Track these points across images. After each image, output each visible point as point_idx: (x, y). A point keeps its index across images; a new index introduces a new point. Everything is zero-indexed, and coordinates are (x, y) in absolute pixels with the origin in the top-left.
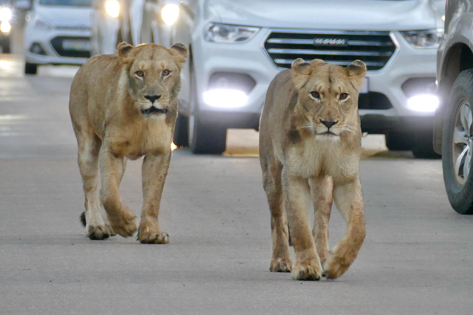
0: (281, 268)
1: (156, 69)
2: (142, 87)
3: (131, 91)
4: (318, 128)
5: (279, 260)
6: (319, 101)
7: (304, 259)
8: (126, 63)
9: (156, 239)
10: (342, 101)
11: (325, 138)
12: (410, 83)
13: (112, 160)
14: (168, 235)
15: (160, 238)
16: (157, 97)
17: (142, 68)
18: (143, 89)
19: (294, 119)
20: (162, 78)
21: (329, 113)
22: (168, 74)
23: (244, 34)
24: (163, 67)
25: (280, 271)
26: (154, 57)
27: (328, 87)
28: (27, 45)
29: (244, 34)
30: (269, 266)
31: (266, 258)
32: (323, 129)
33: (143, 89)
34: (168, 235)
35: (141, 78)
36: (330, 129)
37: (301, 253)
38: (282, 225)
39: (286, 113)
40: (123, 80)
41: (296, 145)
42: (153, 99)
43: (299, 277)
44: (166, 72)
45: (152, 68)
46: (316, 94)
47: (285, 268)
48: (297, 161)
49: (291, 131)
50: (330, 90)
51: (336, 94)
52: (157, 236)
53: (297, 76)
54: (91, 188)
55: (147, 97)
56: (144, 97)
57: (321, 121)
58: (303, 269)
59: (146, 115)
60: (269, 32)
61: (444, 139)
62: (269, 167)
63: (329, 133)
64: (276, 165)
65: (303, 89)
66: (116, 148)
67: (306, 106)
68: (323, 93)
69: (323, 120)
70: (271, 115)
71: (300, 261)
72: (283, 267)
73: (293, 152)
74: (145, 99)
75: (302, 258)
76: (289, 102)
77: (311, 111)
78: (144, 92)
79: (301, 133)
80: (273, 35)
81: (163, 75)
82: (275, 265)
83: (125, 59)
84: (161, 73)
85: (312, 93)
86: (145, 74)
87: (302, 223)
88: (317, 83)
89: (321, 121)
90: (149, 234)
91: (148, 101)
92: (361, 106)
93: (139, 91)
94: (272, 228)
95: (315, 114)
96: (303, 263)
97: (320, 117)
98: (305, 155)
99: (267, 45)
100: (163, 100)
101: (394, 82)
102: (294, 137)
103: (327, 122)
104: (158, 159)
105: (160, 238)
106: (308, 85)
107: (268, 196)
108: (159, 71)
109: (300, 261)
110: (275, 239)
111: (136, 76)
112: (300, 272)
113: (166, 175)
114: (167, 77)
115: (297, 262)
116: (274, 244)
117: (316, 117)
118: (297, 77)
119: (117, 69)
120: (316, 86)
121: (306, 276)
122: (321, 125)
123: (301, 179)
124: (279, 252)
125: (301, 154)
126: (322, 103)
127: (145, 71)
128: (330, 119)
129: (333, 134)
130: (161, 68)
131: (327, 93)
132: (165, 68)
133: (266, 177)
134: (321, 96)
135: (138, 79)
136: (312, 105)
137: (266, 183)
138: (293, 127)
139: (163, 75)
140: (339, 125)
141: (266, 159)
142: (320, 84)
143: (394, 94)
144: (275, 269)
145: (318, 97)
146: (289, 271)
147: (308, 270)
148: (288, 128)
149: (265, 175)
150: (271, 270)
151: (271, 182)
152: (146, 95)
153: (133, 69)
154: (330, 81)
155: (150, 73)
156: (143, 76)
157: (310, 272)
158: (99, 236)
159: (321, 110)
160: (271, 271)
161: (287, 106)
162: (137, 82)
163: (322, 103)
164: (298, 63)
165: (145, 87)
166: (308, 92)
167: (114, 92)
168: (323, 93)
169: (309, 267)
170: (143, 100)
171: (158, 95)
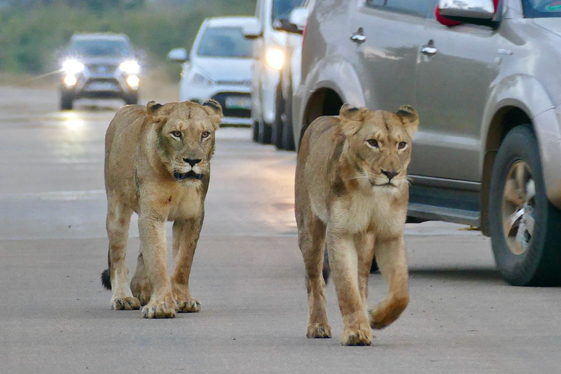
0: (319, 334)
1: (196, 130)
2: (181, 148)
3: (161, 152)
4: (378, 178)
5: (317, 325)
6: (378, 149)
7: (353, 323)
8: (158, 122)
9: (185, 307)
11: (385, 189)
14: (198, 304)
15: (189, 306)
16: (198, 161)
18: (182, 152)
19: (339, 169)
20: (202, 140)
21: (392, 163)
22: (208, 135)
25: (318, 337)
26: (191, 116)
27: (387, 135)
30: (306, 333)
31: (303, 324)
32: (384, 179)
33: (182, 152)
34: (198, 304)
35: (178, 139)
36: (391, 180)
37: (349, 317)
38: (320, 287)
39: (330, 164)
41: (342, 198)
42: (193, 163)
43: (349, 343)
44: (206, 133)
45: (192, 129)
46: (374, 142)
47: (323, 333)
48: (343, 215)
49: (335, 183)
50: (389, 139)
53: (346, 122)
54: (119, 259)
55: (187, 161)
57: (382, 172)
58: (353, 333)
62: (306, 222)
63: (389, 184)
64: (313, 220)
65: (355, 136)
67: (362, 155)
68: (382, 142)
69: (385, 170)
70: (307, 165)
71: (349, 325)
72: (321, 332)
73: (338, 206)
74: (184, 162)
75: (350, 322)
76: (332, 152)
77: (367, 160)
78: (184, 154)
79: (347, 184)
81: (202, 137)
82: (312, 331)
84: (201, 134)
85: (369, 141)
86: (183, 134)
87: (350, 284)
89: (382, 172)
91: (187, 164)
93: (175, 153)
94: (309, 291)
95: (373, 164)
96: (352, 327)
97: (381, 168)
98: (351, 209)
100: (203, 165)
102: (339, 189)
103: (389, 172)
105: (189, 306)
106: (363, 132)
107: (304, 255)
108: (199, 132)
109: (349, 325)
110: (312, 303)
111: (172, 135)
112: (350, 337)
113: (196, 241)
114: (206, 139)
115: (346, 327)
116: (311, 308)
117: (375, 166)
118: (347, 124)
120: (374, 134)
121: (357, 341)
122: (383, 175)
123: (345, 234)
124: (318, 316)
125: (348, 208)
126: (381, 152)
128: (394, 170)
129: (393, 185)
130: (201, 129)
131: (386, 141)
132: (206, 129)
133: (302, 234)
134: (380, 144)
136: (369, 154)
137: (302, 241)
138: (339, 178)
139: (202, 137)
140: (401, 176)
141: (302, 215)
142: (379, 132)
144: (313, 335)
146: (326, 337)
147: (358, 335)
148: (333, 179)
149: (301, 232)
150: (308, 336)
151: (308, 239)
152: (186, 158)
153: (167, 129)
155: (190, 134)
156: (180, 136)
157: (361, 337)
159: (381, 159)
160: (308, 337)
161: (330, 157)
162: (173, 143)
163: (381, 152)
164: (347, 109)
165: (185, 149)
166: (365, 140)
168: (382, 142)
169: (359, 331)
171: (200, 158)
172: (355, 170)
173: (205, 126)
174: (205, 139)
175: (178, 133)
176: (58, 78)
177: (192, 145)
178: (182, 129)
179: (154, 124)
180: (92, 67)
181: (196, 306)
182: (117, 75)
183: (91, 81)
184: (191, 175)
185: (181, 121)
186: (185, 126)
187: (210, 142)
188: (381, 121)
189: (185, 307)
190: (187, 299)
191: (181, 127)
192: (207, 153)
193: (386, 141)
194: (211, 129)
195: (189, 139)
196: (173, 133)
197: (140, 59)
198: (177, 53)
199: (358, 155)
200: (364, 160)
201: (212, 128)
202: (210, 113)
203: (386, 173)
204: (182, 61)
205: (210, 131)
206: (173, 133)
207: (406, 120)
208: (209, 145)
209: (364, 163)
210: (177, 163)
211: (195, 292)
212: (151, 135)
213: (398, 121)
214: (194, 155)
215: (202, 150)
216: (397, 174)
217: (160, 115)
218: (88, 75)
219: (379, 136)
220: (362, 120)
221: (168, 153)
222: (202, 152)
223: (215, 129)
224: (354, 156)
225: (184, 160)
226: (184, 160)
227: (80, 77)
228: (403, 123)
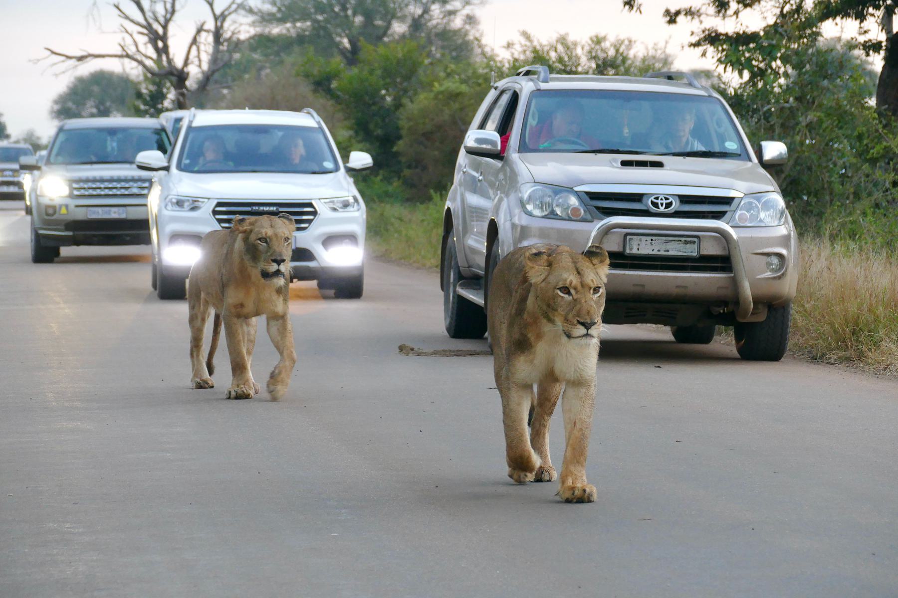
8: (244, 232)
12: (329, 240)
23: (197, 204)
28: (517, 87)
29: (197, 204)
32: (582, 330)
35: (265, 244)
50: (583, 285)
57: (579, 322)
60: (215, 202)
63: (587, 335)
69: (582, 321)
80: (219, 204)
88: (565, 275)
89: (579, 322)
92: (294, 259)
93: (263, 257)
98: (535, 362)
99: (215, 213)
101: (317, 239)
106: (552, 279)
120: (566, 280)
126: (575, 300)
131: (579, 287)
134: (573, 291)
143: (318, 250)
145: (569, 293)
148: (517, 336)
153: (253, 237)
154: (579, 273)
156: (266, 242)
162: (260, 248)
166: (555, 288)
168: (575, 289)
172: (544, 321)
179: (240, 235)
188: (571, 265)
193: (579, 287)
196: (260, 239)
197: (470, 207)
199: (549, 306)
200: (556, 310)
203: (583, 324)
206: (260, 239)
207: (595, 261)
209: (556, 313)
212: (239, 244)
213: (588, 264)
216: (594, 324)
219: (571, 284)
220: (550, 264)
224: (545, 307)
228: (594, 265)
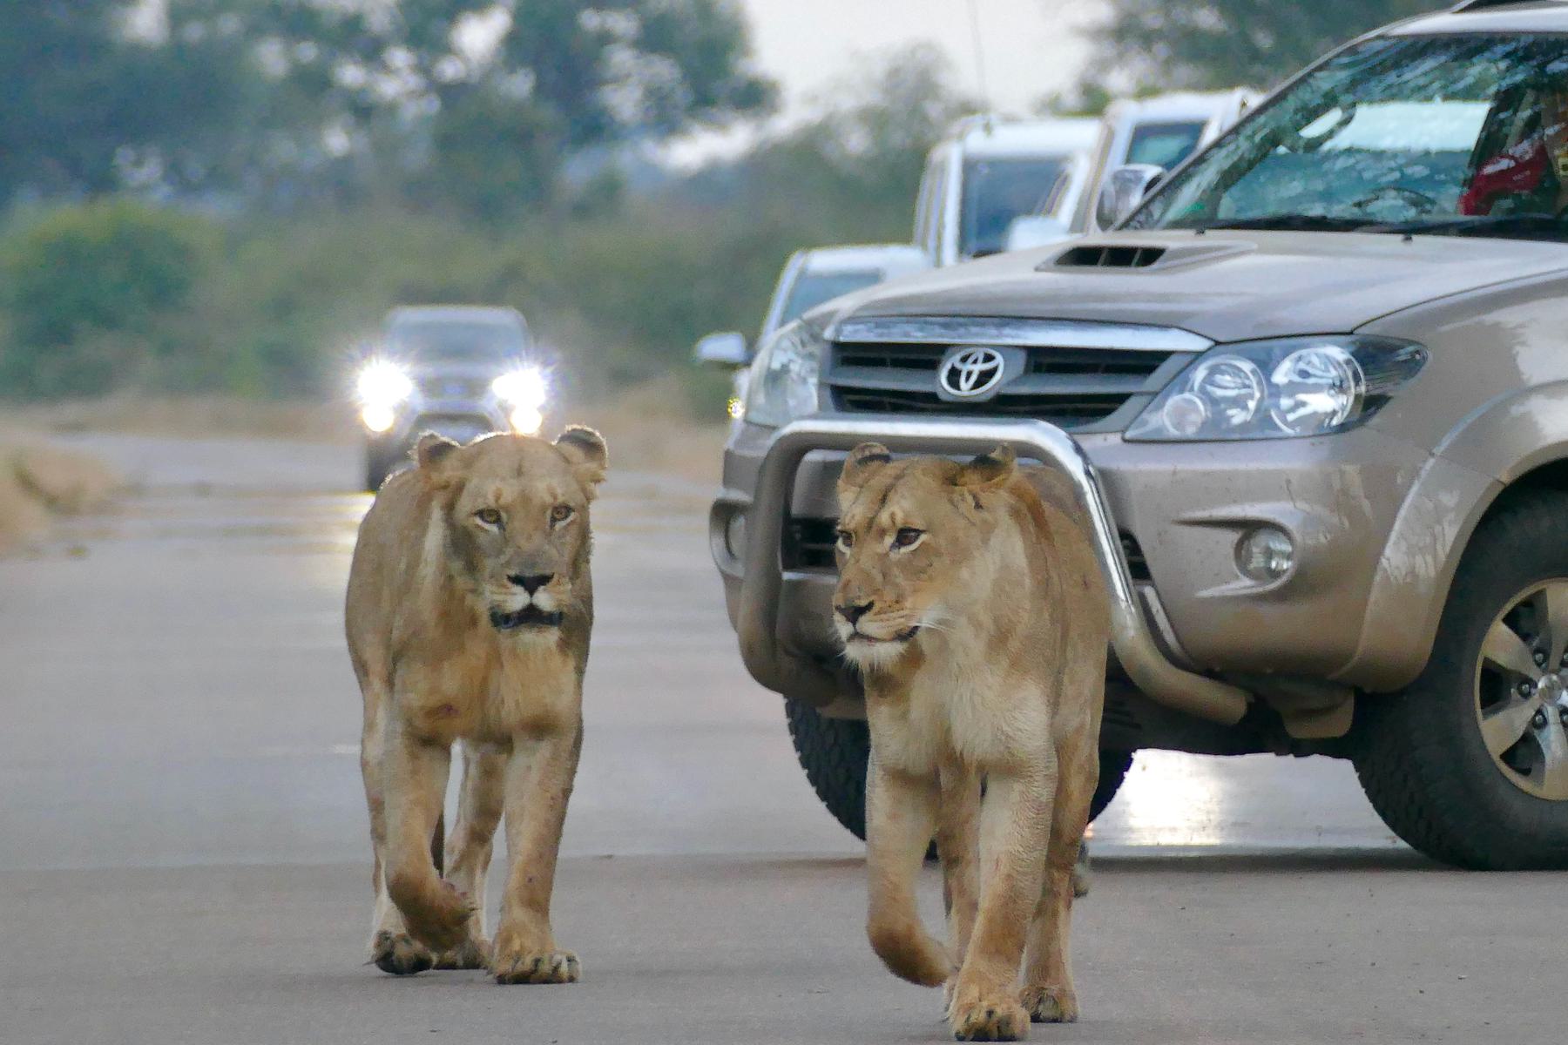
2: (500, 552)
3: (457, 565)
8: (445, 487)
10: (904, 550)
13: (414, 757)
14: (570, 960)
16: (544, 580)
17: (497, 501)
18: (503, 559)
20: (552, 526)
24: (555, 498)
33: (503, 559)
34: (570, 960)
35: (494, 528)
40: (435, 537)
45: (525, 498)
51: (882, 533)
52: (537, 961)
55: (517, 580)
56: (506, 581)
59: (506, 631)
61: (1363, 67)
66: (422, 724)
74: (509, 584)
78: (508, 564)
81: (554, 520)
83: (437, 478)
84: (549, 513)
86: (504, 515)
90: (518, 957)
91: (519, 589)
93: (489, 564)
104: (544, 749)
108: (543, 509)
111: (478, 521)
119: (423, 503)
127: (507, 509)
130: (548, 499)
132: (561, 499)
135: (482, 529)
139: (554, 520)
152: (512, 573)
153: (465, 505)
156: (498, 521)
158: (404, 962)
162: (482, 539)
165: (509, 551)
167: (413, 565)
170: (504, 586)
171: (548, 572)
173: (559, 491)
174: (559, 525)
175: (491, 514)
176: (348, 416)
177: (528, 539)
178: (502, 501)
180: (429, 386)
181: (564, 968)
182: (486, 405)
183: (424, 420)
184: (531, 616)
185: (498, 484)
186: (509, 493)
187: (574, 530)
189: (534, 971)
190: (542, 951)
191: (498, 498)
192: (567, 556)
194: (575, 499)
195: (517, 525)
196: (480, 514)
198: (721, 346)
201: (580, 498)
202: (575, 459)
204: (731, 367)
205: (572, 504)
208: (570, 539)
210: (494, 589)
211: (567, 932)
214: (533, 565)
215: (554, 552)
217: (449, 470)
218: (420, 404)
221: (472, 568)
222: (556, 556)
223: (588, 500)
225: (509, 578)
226: (509, 578)
227: (402, 410)
